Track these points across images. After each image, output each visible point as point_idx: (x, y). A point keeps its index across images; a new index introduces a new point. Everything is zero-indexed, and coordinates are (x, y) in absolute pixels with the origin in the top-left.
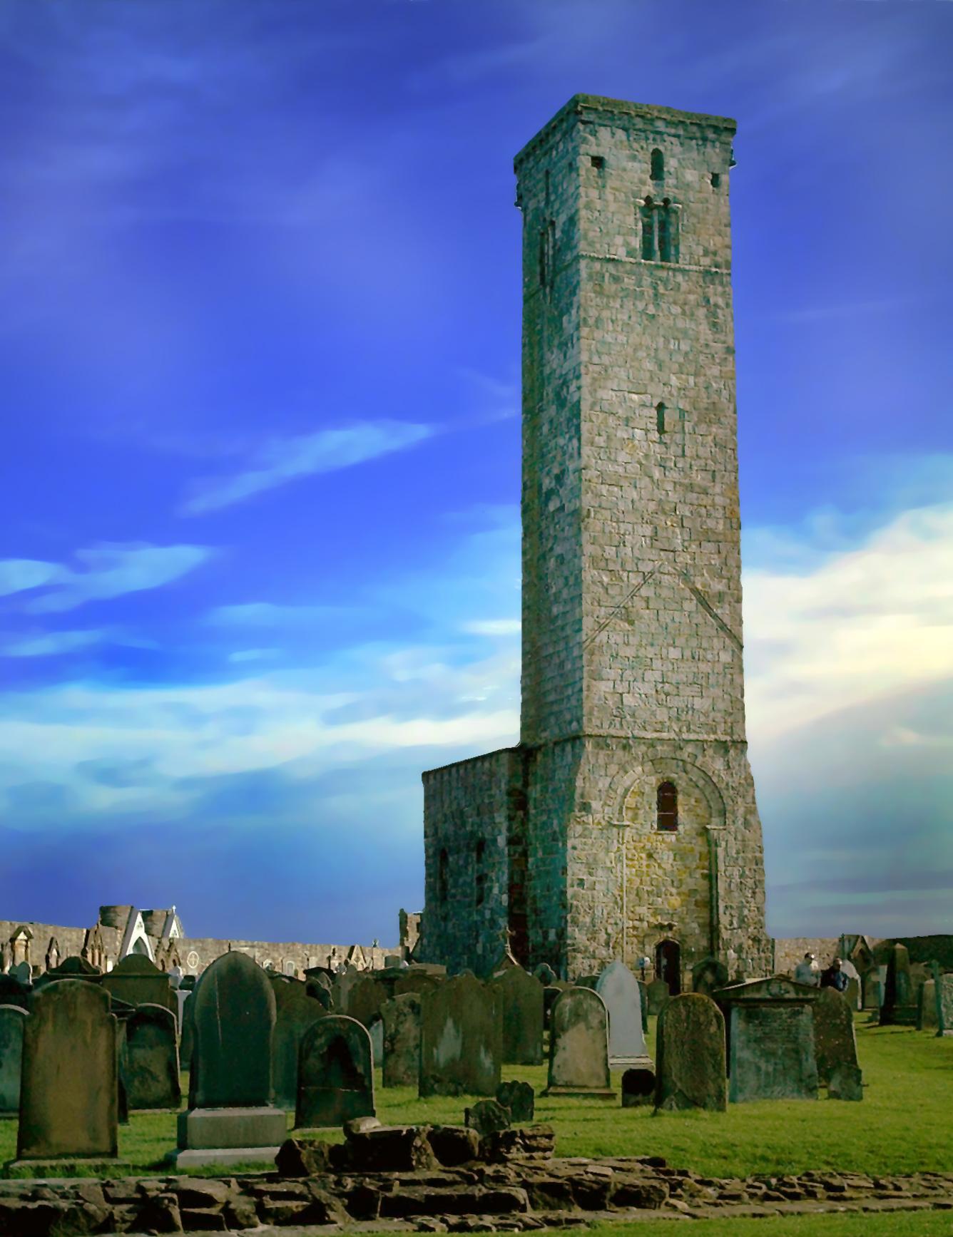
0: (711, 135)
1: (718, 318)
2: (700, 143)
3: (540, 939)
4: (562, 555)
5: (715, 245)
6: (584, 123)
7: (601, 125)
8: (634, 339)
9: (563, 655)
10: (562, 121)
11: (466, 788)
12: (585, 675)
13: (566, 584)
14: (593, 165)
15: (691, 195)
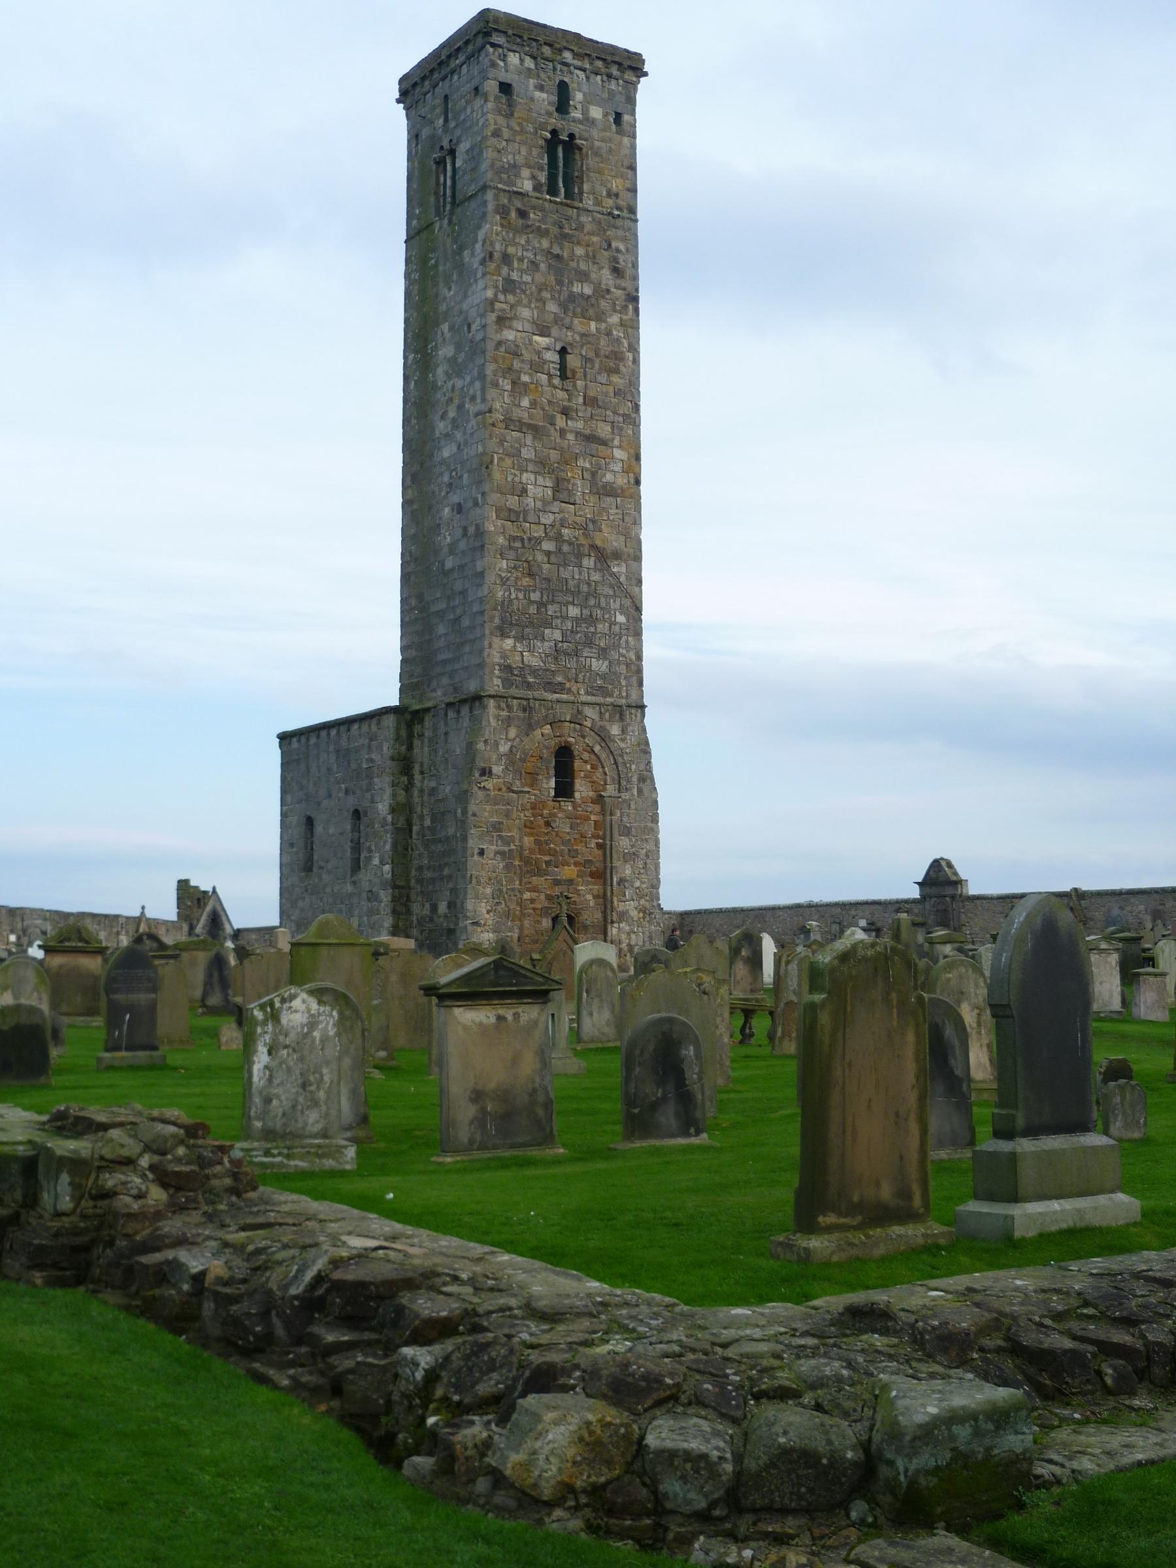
0: (614, 71)
1: (618, 263)
2: (605, 78)
3: (426, 911)
4: (459, 504)
5: (617, 186)
6: (493, 45)
7: (509, 50)
8: (539, 278)
9: (459, 612)
10: (467, 43)
11: (338, 751)
12: (487, 632)
13: (465, 534)
14: (500, 92)
15: (595, 133)
